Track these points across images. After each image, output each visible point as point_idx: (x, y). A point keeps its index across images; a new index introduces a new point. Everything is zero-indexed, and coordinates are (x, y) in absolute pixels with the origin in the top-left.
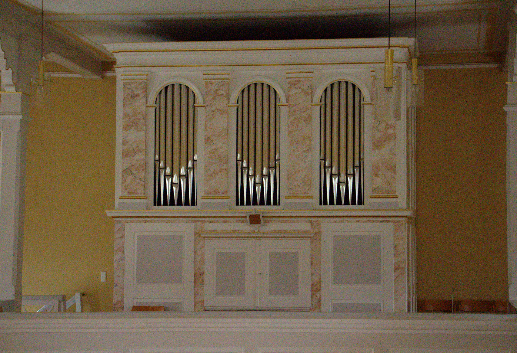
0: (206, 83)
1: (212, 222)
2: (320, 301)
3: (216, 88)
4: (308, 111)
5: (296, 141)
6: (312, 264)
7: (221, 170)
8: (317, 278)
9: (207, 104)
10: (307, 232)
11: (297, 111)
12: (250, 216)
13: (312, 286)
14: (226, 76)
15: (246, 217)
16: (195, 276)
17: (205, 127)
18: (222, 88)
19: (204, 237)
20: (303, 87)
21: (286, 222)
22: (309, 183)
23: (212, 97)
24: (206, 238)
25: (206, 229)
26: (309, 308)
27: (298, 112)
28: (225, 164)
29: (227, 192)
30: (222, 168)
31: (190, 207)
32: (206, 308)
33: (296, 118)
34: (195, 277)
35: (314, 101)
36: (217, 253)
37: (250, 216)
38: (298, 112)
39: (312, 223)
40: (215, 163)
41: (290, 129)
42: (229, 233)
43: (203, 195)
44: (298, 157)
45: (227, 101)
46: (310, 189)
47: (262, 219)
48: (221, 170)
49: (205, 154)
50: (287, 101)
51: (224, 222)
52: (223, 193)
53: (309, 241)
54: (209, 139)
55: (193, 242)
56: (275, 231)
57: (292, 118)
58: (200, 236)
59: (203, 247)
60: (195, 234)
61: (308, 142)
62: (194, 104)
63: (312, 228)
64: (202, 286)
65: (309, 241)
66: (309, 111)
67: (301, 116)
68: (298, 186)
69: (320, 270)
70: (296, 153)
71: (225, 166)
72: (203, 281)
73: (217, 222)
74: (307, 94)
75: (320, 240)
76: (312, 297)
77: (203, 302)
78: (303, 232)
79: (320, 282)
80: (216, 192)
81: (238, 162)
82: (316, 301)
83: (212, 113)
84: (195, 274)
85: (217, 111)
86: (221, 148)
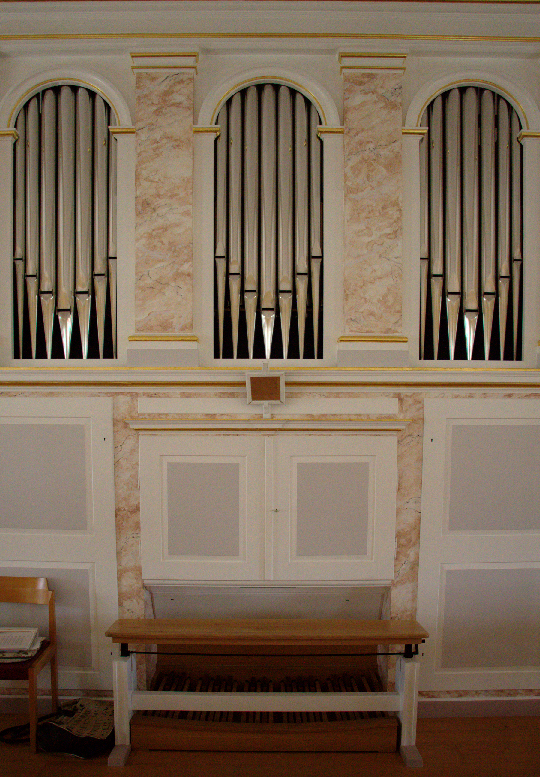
0: (139, 78)
1: (156, 395)
2: (415, 564)
3: (164, 87)
4: (394, 145)
5: (366, 210)
6: (399, 489)
7: (178, 275)
8: (409, 519)
9: (140, 125)
10: (389, 418)
11: (368, 142)
12: (254, 380)
13: (399, 535)
14: (190, 61)
15: (243, 384)
16: (117, 515)
17: (137, 178)
18: (177, 88)
19: (137, 430)
20: (381, 91)
21: (338, 395)
22: (398, 308)
23: (155, 108)
24: (141, 432)
25: (140, 410)
26: (390, 582)
27: (371, 146)
28: (186, 261)
29: (191, 326)
30: (179, 271)
31: (101, 362)
32: (145, 582)
33: (363, 160)
34: (119, 517)
35: (407, 126)
36: (299, 465)
37: (254, 380)
38: (371, 146)
39: (401, 400)
40: (162, 261)
41: (349, 184)
42: (196, 420)
43: (132, 333)
44: (369, 247)
45: (191, 120)
46: (400, 322)
47: (283, 389)
48: (178, 275)
49: (138, 240)
50: (343, 120)
51: (183, 395)
52: (182, 330)
53: (392, 440)
54: (146, 204)
55: (110, 439)
56: (311, 415)
57: (355, 159)
58: (126, 425)
59: (134, 451)
60: (115, 422)
61: (396, 215)
62: (109, 124)
63: (401, 410)
64: (135, 535)
65: (392, 440)
66: (398, 144)
67: (377, 156)
68: (372, 314)
69: (418, 501)
70: (367, 239)
71: (186, 268)
72: (137, 526)
73: (167, 396)
74: (392, 106)
75: (420, 436)
76: (397, 559)
77: (138, 571)
78: (381, 418)
79: (417, 527)
80: (165, 326)
81: (217, 260)
82: (405, 568)
83: (155, 145)
84: (118, 510)
85: (165, 141)
86: (177, 225)
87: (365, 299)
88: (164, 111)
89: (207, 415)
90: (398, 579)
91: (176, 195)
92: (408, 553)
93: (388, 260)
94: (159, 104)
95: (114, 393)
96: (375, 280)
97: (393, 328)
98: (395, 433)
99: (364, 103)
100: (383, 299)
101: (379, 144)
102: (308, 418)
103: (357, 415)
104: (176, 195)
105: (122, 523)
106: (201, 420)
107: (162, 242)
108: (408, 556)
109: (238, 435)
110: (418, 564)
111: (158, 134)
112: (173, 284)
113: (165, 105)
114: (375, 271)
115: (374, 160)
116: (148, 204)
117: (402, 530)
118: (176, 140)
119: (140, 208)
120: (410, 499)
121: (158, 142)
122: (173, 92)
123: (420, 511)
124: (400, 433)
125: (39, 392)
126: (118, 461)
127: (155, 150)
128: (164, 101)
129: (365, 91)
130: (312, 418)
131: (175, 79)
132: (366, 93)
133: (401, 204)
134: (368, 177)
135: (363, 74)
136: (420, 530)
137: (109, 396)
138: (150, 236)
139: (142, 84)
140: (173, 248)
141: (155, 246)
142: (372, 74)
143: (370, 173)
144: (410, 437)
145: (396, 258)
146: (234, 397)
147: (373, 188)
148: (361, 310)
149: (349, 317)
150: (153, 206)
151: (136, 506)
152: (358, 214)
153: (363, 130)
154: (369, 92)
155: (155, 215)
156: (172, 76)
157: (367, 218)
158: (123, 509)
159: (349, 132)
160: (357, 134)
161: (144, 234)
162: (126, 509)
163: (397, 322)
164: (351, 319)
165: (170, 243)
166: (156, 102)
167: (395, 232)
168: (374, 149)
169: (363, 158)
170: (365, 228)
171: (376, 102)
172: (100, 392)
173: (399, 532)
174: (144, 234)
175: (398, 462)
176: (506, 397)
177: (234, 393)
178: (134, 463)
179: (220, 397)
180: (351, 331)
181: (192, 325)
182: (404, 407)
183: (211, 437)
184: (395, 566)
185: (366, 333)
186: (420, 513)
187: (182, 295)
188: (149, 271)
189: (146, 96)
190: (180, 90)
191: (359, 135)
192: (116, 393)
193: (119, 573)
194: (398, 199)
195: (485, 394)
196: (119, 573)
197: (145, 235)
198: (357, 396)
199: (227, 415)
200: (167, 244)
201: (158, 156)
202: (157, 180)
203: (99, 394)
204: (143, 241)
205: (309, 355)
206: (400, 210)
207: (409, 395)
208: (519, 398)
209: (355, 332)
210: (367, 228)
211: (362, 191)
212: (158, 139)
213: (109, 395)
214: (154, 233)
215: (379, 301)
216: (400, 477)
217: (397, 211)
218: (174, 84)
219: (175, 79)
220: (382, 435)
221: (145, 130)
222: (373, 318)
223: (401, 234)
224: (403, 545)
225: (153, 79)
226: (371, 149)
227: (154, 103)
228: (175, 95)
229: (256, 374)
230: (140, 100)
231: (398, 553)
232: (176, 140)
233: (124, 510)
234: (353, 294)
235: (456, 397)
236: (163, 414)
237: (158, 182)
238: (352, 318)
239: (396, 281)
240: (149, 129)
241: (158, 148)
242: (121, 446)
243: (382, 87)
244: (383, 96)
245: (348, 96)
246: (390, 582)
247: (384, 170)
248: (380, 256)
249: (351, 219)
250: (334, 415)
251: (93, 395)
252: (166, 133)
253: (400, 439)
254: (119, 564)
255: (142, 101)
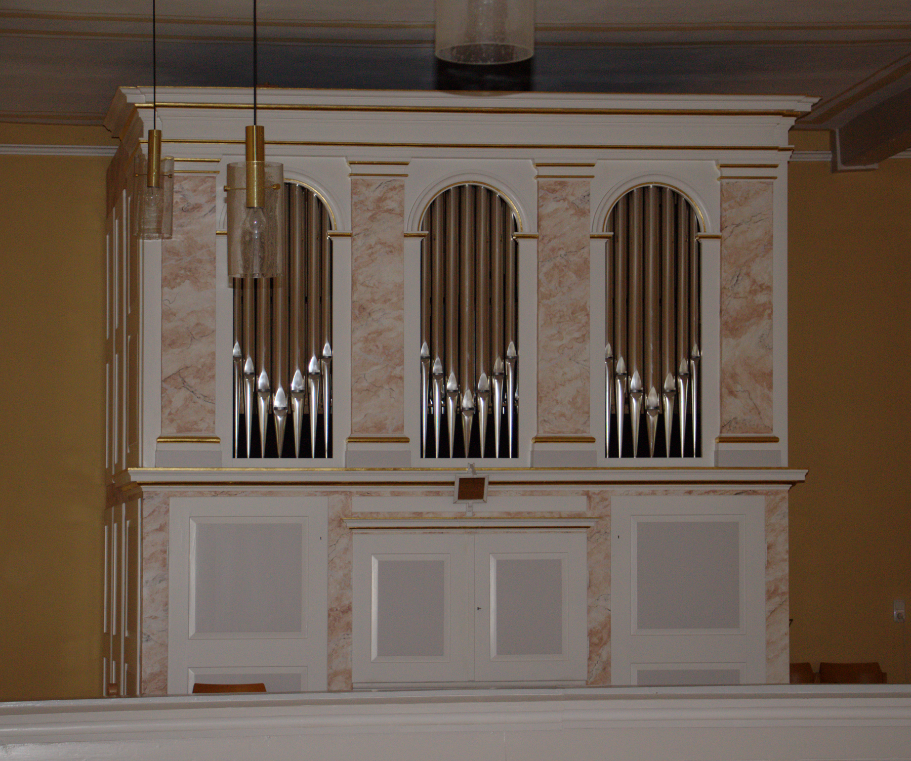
0: (354, 185)
3: (378, 194)
6: (589, 586)
7: (391, 378)
11: (560, 249)
12: (461, 480)
13: (591, 634)
15: (453, 483)
17: (354, 283)
18: (390, 194)
20: (571, 198)
23: (370, 214)
24: (354, 531)
27: (562, 252)
30: (392, 374)
33: (555, 266)
34: (331, 618)
37: (461, 480)
40: (377, 364)
48: (391, 378)
51: (393, 494)
52: (394, 431)
53: (580, 537)
54: (362, 308)
56: (508, 513)
64: (346, 636)
66: (586, 250)
67: (567, 262)
68: (563, 415)
71: (397, 371)
72: (349, 626)
76: (590, 659)
79: (607, 625)
83: (370, 251)
85: (379, 246)
87: (557, 400)
88: (378, 217)
89: (414, 513)
90: (592, 680)
91: (389, 300)
92: (600, 652)
93: (577, 363)
94: (374, 210)
95: (329, 492)
96: (565, 383)
97: (582, 429)
98: (584, 530)
99: (556, 210)
100: (573, 400)
101: (569, 250)
102: (505, 516)
103: (550, 512)
104: (389, 300)
105: (334, 624)
106: (409, 518)
107: (377, 346)
108: (600, 656)
109: (442, 533)
110: (610, 664)
111: (372, 240)
112: (387, 387)
113: (379, 211)
114: (565, 374)
115: (565, 266)
116: (364, 308)
117: (594, 628)
118: (389, 246)
119: (357, 312)
120: (599, 596)
121: (373, 248)
122: (386, 199)
123: (610, 609)
124: (589, 529)
125: (258, 491)
126: (332, 560)
127: (370, 256)
128: (379, 207)
129: (557, 199)
130: (511, 516)
131: (387, 186)
132: (559, 201)
133: (588, 309)
134: (560, 283)
135: (556, 182)
136: (610, 629)
137: (325, 495)
138: (366, 340)
139: (358, 190)
140: (387, 352)
141: (370, 350)
142: (563, 182)
143: (561, 279)
144: (598, 534)
145: (584, 361)
146: (439, 495)
147: (564, 294)
148: (554, 411)
149: (542, 419)
150: (368, 311)
151: (347, 606)
152: (551, 318)
153: (555, 237)
154: (561, 200)
155: (370, 319)
156: (386, 183)
157: (558, 323)
158: (335, 610)
159: (543, 239)
160: (550, 241)
161: (361, 338)
162: (339, 609)
163: (585, 423)
164: (544, 420)
165: (384, 347)
166: (371, 208)
167: (584, 336)
168: (565, 255)
169: (555, 264)
170: (556, 332)
171: (567, 209)
172: (316, 492)
173: (591, 630)
174: (361, 338)
175: (588, 559)
176: (686, 494)
177: (439, 492)
178: (347, 562)
179: (426, 495)
180: (545, 432)
181: (403, 426)
182: (592, 504)
183: (418, 535)
184: (588, 666)
185: (558, 433)
186: (610, 610)
187: (394, 397)
188: (365, 374)
189: (362, 202)
190: (392, 197)
191: (552, 242)
192: (331, 492)
193: (330, 677)
194: (586, 303)
195: (666, 491)
196: (330, 677)
197: (362, 339)
198: (549, 494)
199: (433, 513)
200: (381, 348)
201: (373, 261)
202: (372, 285)
203: (316, 493)
204: (360, 345)
205: (504, 454)
206: (588, 315)
207: (597, 492)
208: (699, 494)
209: (549, 432)
210: (558, 332)
211: (554, 296)
212: (373, 244)
213: (325, 494)
214: (370, 337)
215: (569, 402)
216: (591, 574)
217: (585, 316)
218: (387, 190)
219: (387, 186)
220: (573, 532)
221: (361, 235)
222: (563, 419)
223: (589, 338)
224: (595, 644)
225: (368, 185)
226: (562, 256)
227: (369, 209)
228: (388, 202)
229: (464, 476)
230: (356, 206)
231: (591, 652)
232: (389, 246)
233: (337, 610)
234: (546, 396)
235: (640, 494)
236: (375, 513)
237: (373, 287)
238: (546, 419)
239: (585, 384)
240: (364, 235)
241: (372, 253)
242: (335, 545)
243: (572, 195)
244: (573, 203)
245: (542, 203)
246: (585, 682)
247: (574, 277)
248: (570, 359)
249: (544, 324)
250: (529, 513)
251: (310, 495)
252: (380, 239)
253: (589, 536)
254: (330, 667)
255: (358, 207)
